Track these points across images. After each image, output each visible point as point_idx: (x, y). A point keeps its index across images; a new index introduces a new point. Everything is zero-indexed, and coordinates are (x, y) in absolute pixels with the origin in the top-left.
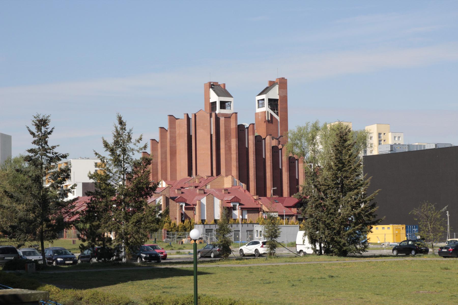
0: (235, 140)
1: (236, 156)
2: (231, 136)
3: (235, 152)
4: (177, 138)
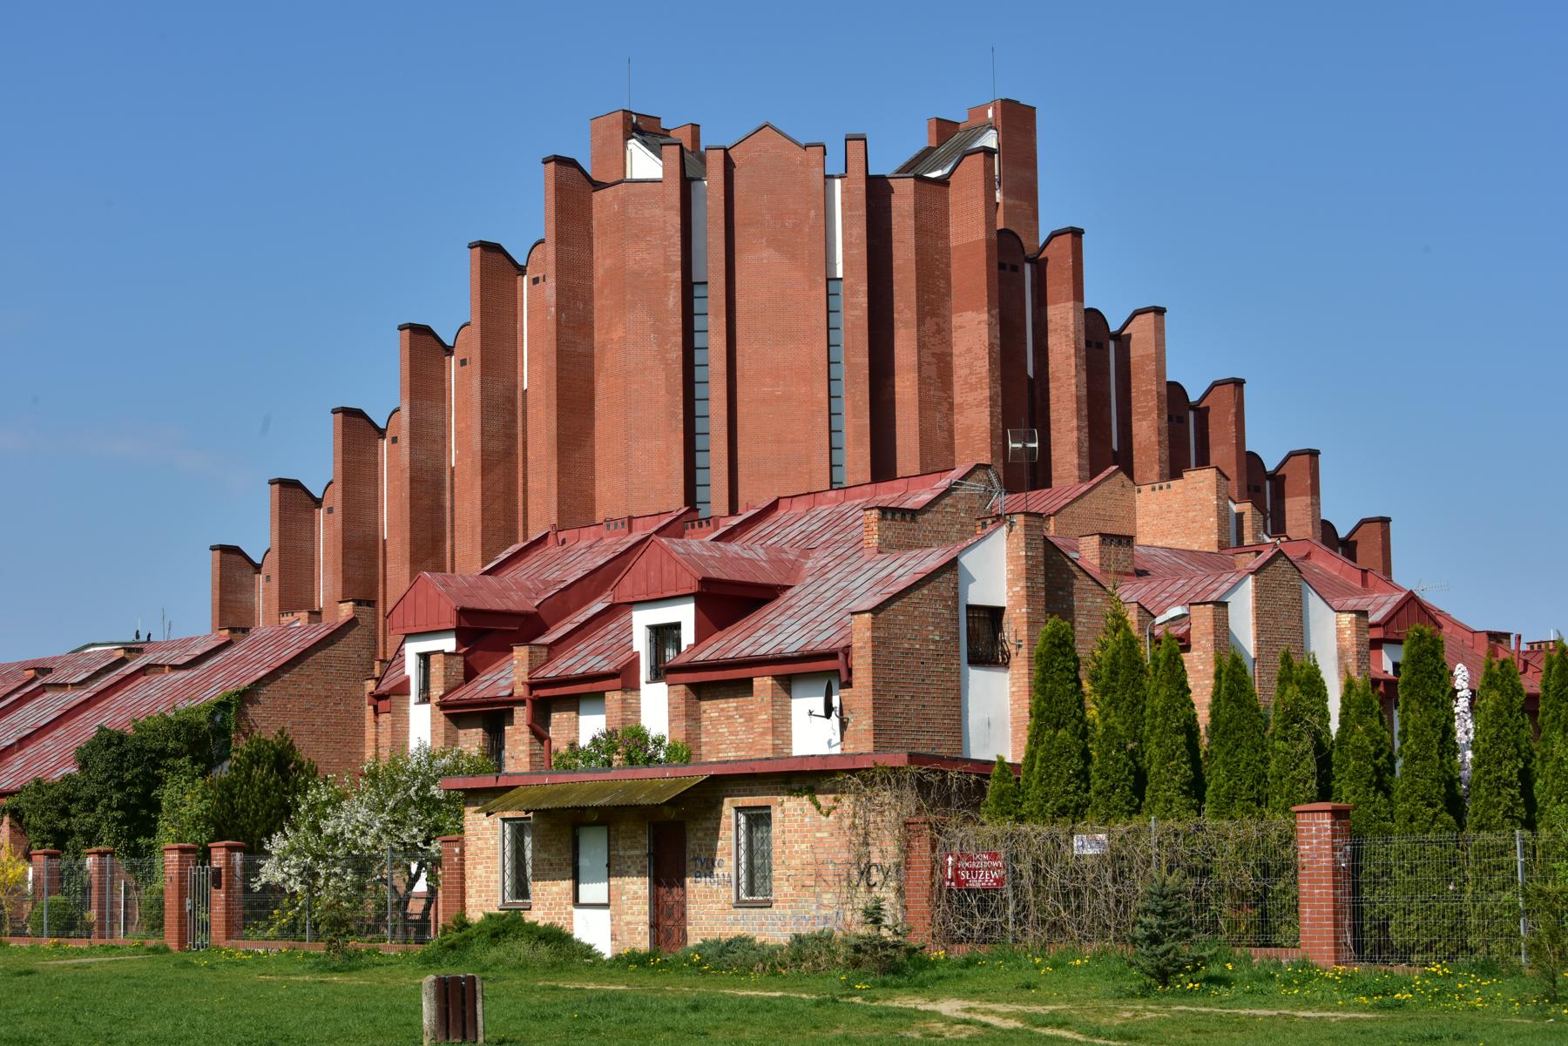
0: (985, 316)
1: (992, 415)
2: (948, 293)
3: (987, 393)
4: (597, 303)
